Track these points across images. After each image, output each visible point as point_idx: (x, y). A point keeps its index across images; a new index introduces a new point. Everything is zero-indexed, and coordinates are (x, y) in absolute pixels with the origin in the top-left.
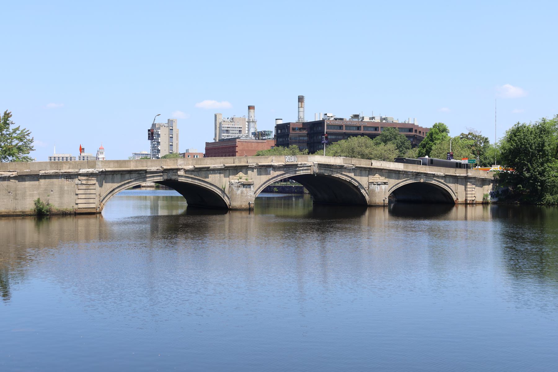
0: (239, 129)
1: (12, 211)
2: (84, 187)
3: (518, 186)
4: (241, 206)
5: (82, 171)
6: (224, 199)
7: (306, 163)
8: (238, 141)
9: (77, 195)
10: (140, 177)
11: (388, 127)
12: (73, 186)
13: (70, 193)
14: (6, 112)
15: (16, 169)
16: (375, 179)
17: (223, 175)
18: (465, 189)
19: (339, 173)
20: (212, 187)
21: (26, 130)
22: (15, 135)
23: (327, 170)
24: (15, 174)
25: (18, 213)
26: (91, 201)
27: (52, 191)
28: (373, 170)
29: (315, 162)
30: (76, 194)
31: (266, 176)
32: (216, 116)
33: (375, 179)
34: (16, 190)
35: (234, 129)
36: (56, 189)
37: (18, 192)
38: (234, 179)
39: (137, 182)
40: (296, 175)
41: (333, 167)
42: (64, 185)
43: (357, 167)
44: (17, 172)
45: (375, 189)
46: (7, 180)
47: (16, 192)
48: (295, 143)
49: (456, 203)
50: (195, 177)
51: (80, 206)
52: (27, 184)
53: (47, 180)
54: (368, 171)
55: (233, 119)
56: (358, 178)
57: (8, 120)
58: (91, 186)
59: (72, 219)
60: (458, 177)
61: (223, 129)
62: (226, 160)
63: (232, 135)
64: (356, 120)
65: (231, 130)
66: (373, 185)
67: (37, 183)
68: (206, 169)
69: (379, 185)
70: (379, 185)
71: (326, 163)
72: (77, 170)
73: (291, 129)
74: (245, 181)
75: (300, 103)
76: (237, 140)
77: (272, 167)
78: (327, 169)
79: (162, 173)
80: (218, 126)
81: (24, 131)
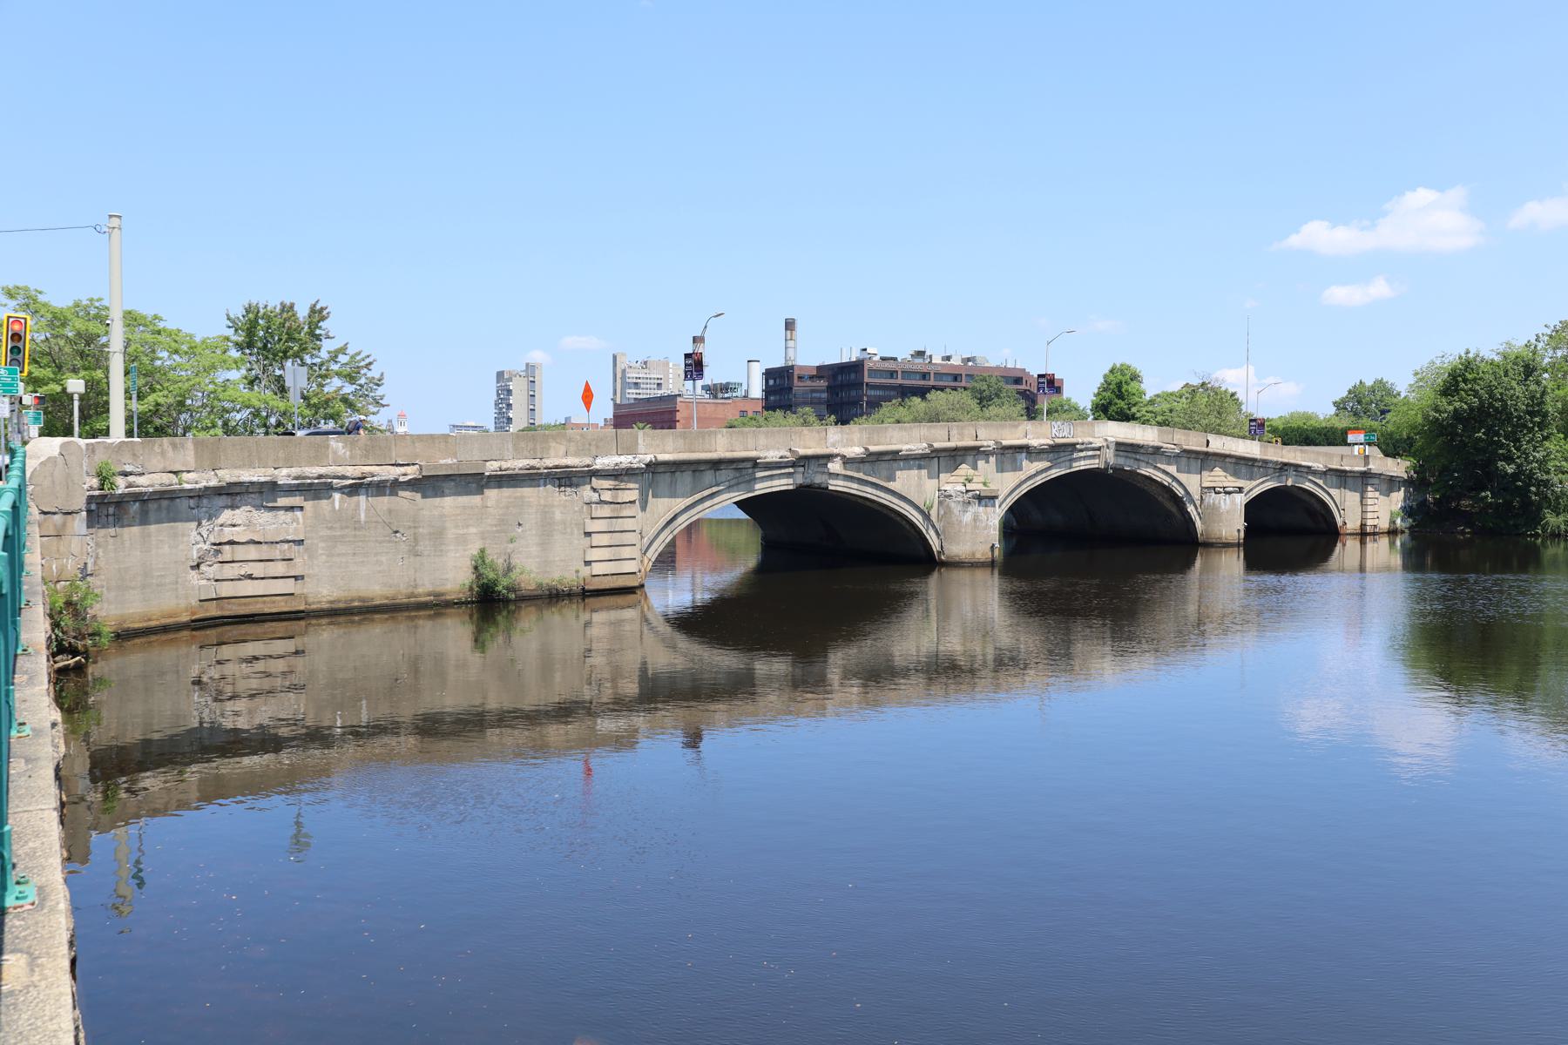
0: (656, 381)
1: (404, 591)
2: (606, 511)
3: (1483, 494)
4: (973, 554)
5: (604, 462)
6: (928, 537)
7: (1091, 440)
8: (681, 402)
9: (588, 534)
10: (741, 480)
11: (985, 375)
12: (576, 509)
13: (569, 530)
14: (315, 305)
15: (417, 456)
16: (1216, 479)
17: (926, 471)
18: (1361, 502)
19: (1152, 465)
20: (902, 504)
21: (362, 355)
22: (335, 367)
23: (1130, 458)
24: (412, 472)
25: (423, 599)
26: (626, 552)
27: (520, 525)
28: (1210, 458)
29: (1110, 439)
30: (585, 533)
31: (1012, 473)
32: (615, 358)
33: (1216, 479)
34: (416, 525)
35: (648, 381)
36: (531, 518)
37: (421, 530)
38: (952, 483)
39: (732, 495)
40: (1072, 470)
41: (1142, 451)
42: (553, 506)
43: (1185, 451)
44: (417, 466)
45: (1220, 503)
46: (388, 492)
47: (417, 531)
48: (805, 404)
49: (1342, 532)
50: (866, 478)
51: (598, 569)
52: (449, 504)
53: (507, 492)
54: (1202, 460)
55: (645, 363)
56: (1182, 477)
57: (320, 328)
58: (625, 508)
59: (574, 606)
60: (1349, 474)
61: (628, 380)
62: (933, 431)
63: (645, 391)
64: (921, 361)
65: (643, 383)
66: (1213, 494)
67: (475, 500)
68: (889, 457)
69: (1229, 493)
70: (1229, 493)
71: (1130, 441)
72: (588, 461)
73: (796, 377)
74: (981, 487)
75: (789, 332)
76: (679, 399)
77: (1025, 450)
78: (1129, 455)
79: (792, 467)
80: (619, 375)
81: (358, 358)
